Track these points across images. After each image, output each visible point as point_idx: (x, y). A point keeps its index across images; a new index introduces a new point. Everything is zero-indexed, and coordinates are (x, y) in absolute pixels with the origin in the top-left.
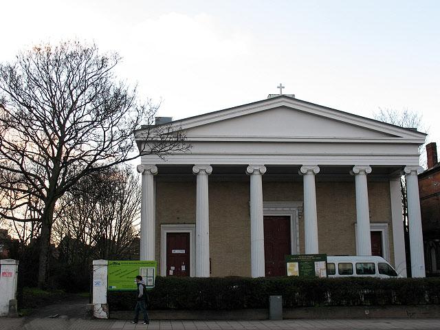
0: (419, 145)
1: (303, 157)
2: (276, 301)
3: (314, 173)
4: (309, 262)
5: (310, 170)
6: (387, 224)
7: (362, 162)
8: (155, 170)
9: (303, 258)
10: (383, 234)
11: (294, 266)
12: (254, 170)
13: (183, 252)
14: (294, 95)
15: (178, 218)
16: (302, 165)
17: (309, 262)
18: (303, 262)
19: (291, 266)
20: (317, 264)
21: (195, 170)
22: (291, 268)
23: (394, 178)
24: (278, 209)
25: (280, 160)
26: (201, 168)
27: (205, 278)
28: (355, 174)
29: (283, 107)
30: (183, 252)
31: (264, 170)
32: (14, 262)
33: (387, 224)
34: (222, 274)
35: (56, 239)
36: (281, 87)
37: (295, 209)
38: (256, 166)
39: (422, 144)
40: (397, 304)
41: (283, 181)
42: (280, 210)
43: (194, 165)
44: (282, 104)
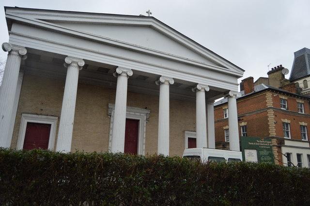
0: (238, 77)
5: (125, 72)
8: (25, 52)
10: (52, 126)
12: (73, 62)
15: (42, 110)
16: (117, 67)
23: (211, 102)
24: (131, 113)
25: (92, 57)
26: (75, 60)
27: (63, 155)
28: (118, 75)
32: (256, 151)
34: (74, 152)
35: (276, 144)
37: (143, 115)
38: (124, 68)
39: (240, 77)
43: (67, 56)
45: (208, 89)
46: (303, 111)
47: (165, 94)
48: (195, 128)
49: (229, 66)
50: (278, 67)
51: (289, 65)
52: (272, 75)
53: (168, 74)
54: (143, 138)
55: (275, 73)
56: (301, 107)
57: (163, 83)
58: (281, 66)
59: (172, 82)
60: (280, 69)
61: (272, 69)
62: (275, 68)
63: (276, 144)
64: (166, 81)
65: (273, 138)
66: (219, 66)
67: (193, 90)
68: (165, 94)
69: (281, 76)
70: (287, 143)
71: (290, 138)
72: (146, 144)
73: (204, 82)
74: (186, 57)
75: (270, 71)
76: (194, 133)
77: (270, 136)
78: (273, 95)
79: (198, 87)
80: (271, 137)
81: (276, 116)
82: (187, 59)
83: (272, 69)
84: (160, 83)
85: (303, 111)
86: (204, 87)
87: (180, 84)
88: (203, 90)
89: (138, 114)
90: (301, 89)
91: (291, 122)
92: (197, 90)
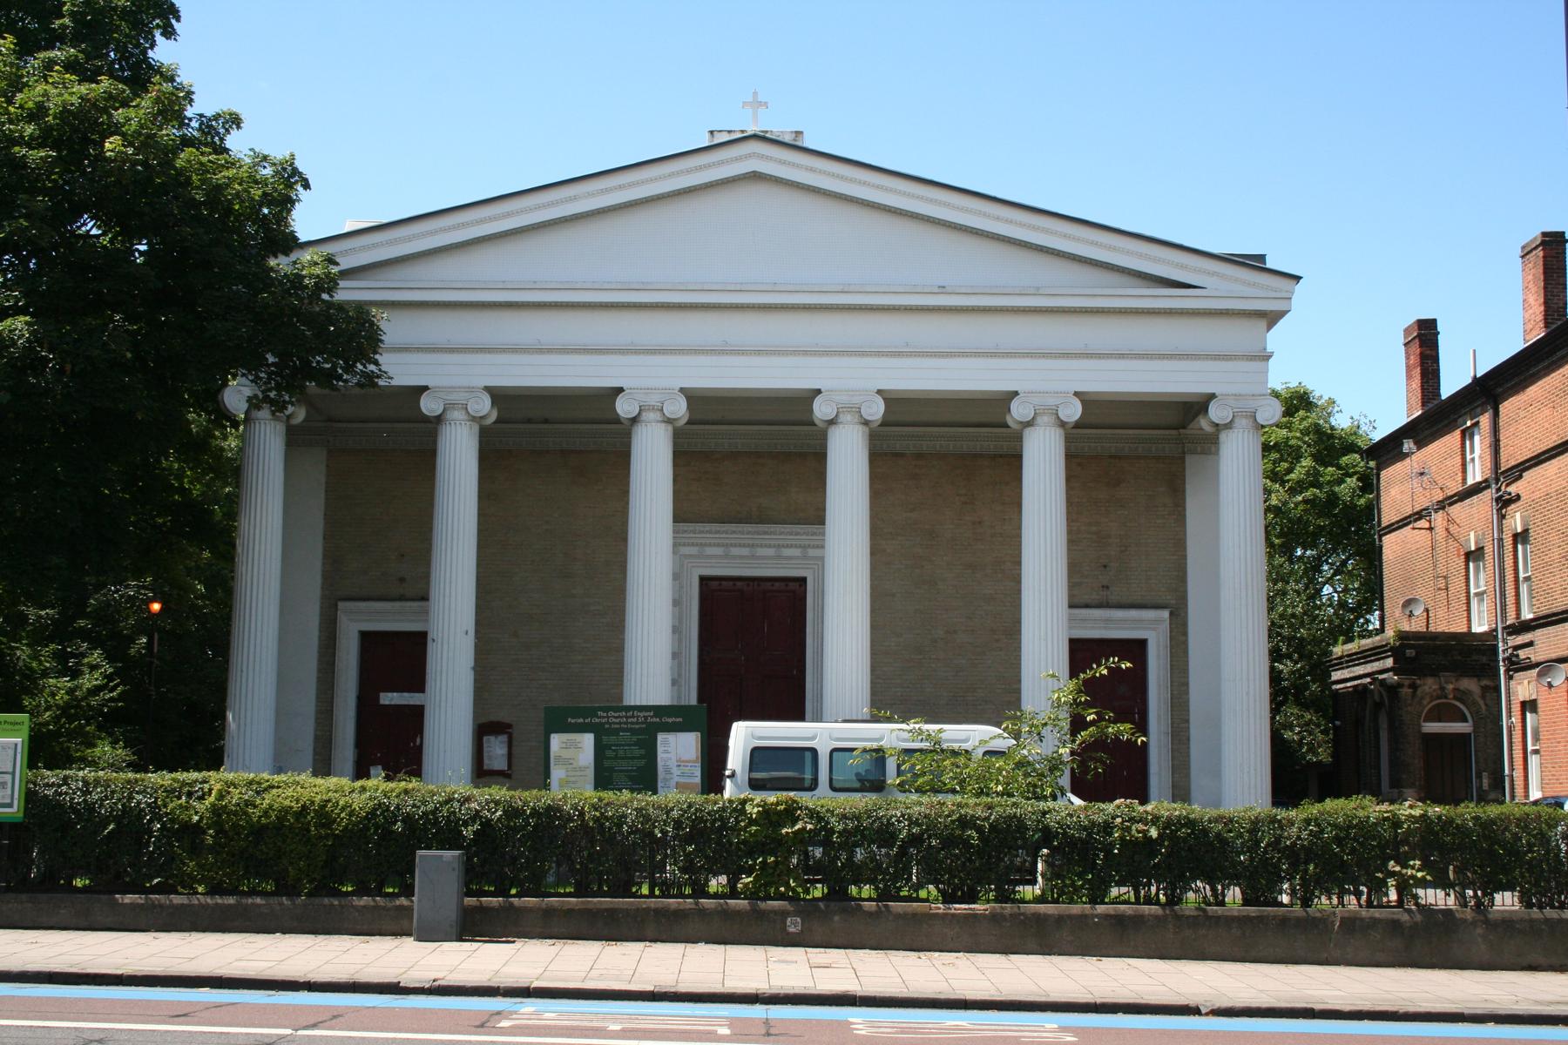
1: (1122, 364)
2: (438, 867)
3: (1063, 424)
4: (633, 732)
6: (1166, 614)
7: (1047, 379)
9: (614, 718)
11: (577, 746)
13: (388, 698)
14: (798, 133)
15: (402, 580)
17: (633, 732)
18: (616, 732)
19: (567, 746)
20: (666, 743)
21: (821, 410)
22: (566, 754)
26: (453, 397)
29: (756, 177)
30: (388, 698)
31: (876, 410)
33: (1166, 614)
36: (757, 104)
40: (1319, 925)
41: (751, 453)
42: (754, 555)
44: (755, 166)
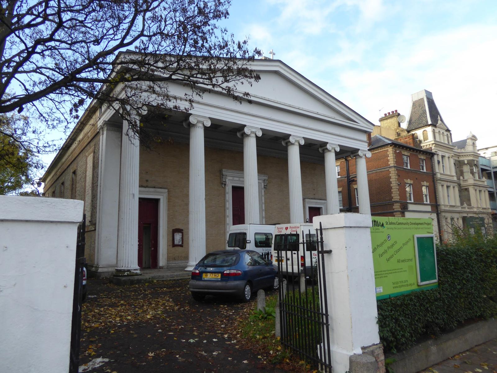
10: (161, 201)
15: (147, 181)
24: (235, 179)
35: (400, 210)
45: (260, 134)
46: (409, 165)
47: (198, 141)
48: (326, 196)
49: (359, 120)
50: (393, 112)
51: (406, 112)
52: (385, 121)
53: (299, 132)
54: (263, 210)
55: (389, 120)
56: (423, 164)
57: (292, 144)
58: (396, 111)
59: (208, 124)
60: (396, 114)
61: (386, 115)
62: (389, 113)
63: (400, 210)
64: (252, 132)
65: (396, 202)
66: (347, 119)
67: (239, 135)
68: (198, 141)
69: (397, 125)
70: (411, 207)
71: (412, 201)
72: (266, 218)
73: (334, 140)
74: (316, 110)
75: (382, 118)
76: (326, 201)
77: (393, 200)
78: (396, 150)
79: (246, 130)
80: (394, 201)
81: (399, 176)
82: (317, 114)
83: (386, 115)
84: (190, 125)
85: (409, 165)
86: (298, 139)
87: (220, 126)
88: (253, 135)
89: (237, 179)
90: (420, 141)
91: (414, 182)
92: (288, 143)
